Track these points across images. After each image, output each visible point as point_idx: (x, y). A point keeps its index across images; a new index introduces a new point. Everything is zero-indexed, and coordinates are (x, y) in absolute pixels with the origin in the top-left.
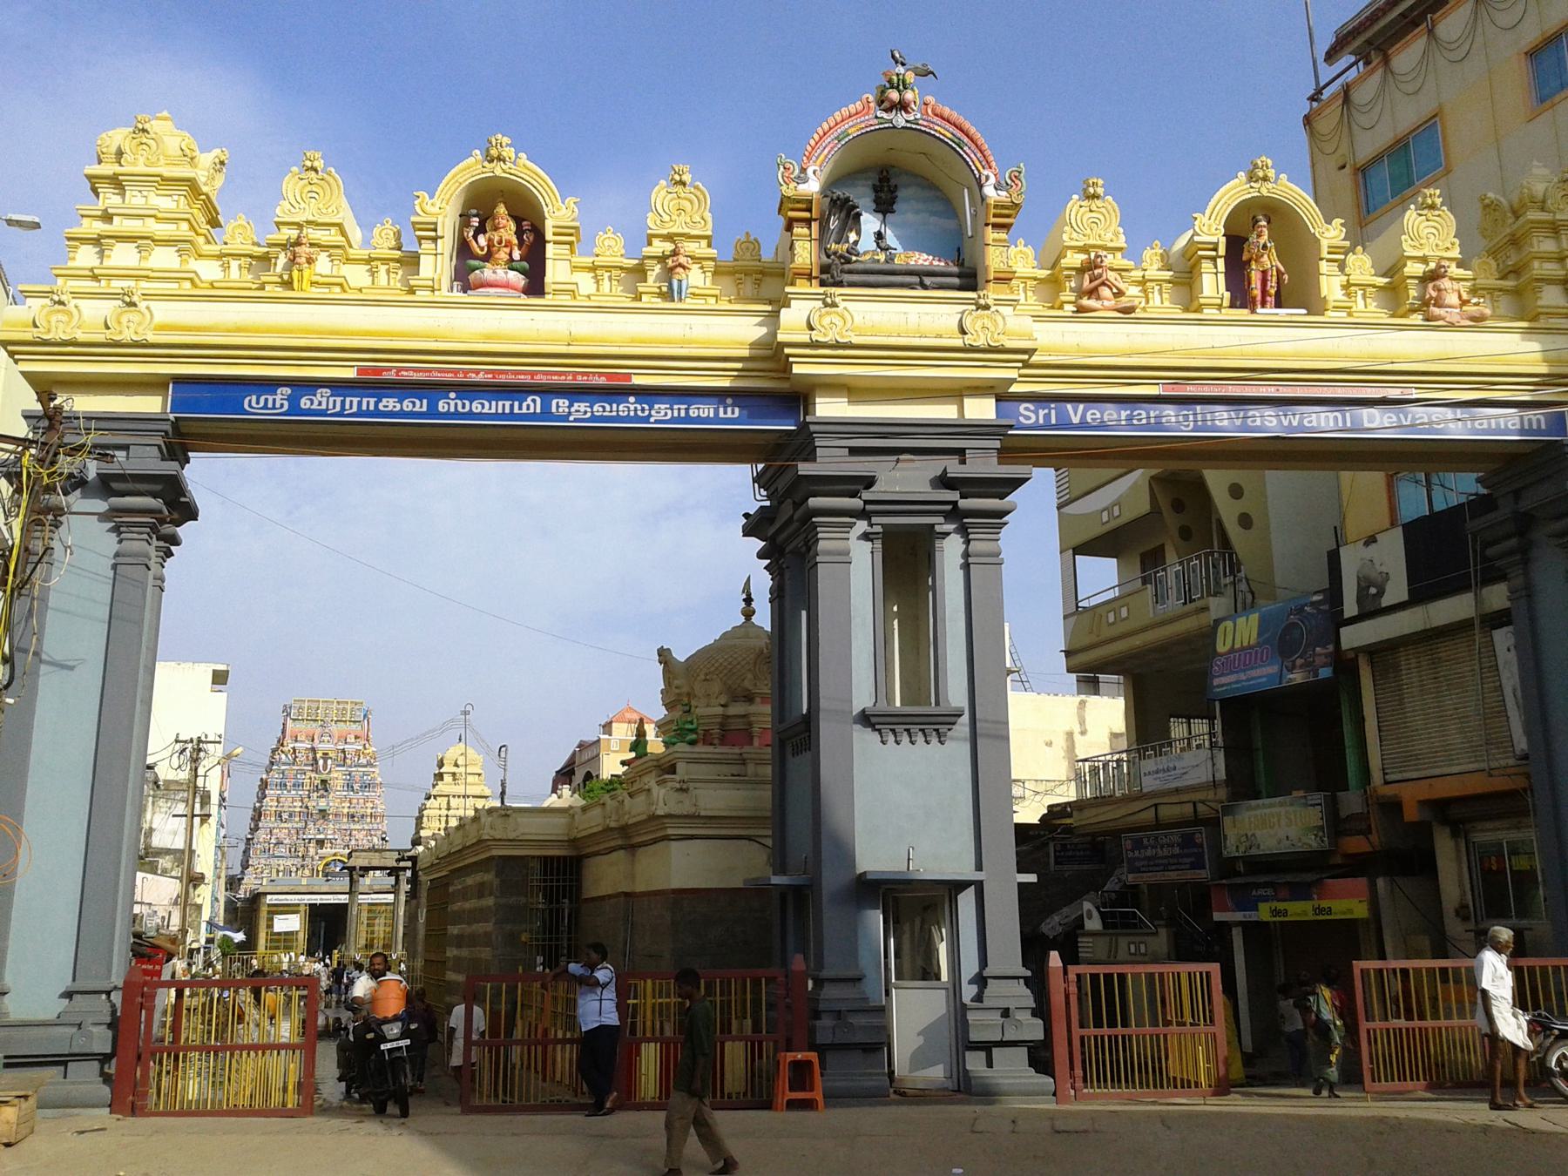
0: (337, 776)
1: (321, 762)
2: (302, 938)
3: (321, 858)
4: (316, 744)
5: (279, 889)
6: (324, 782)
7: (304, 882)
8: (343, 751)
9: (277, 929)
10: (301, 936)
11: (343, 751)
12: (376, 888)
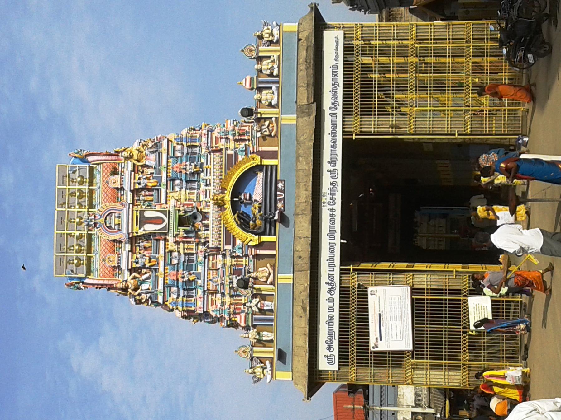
0: (176, 199)
1: (149, 228)
2: (433, 276)
3: (229, 238)
4: (123, 235)
5: (302, 342)
6: (182, 221)
7: (285, 278)
8: (136, 192)
9: (405, 343)
10: (424, 281)
11: (136, 192)
12: (304, 97)
